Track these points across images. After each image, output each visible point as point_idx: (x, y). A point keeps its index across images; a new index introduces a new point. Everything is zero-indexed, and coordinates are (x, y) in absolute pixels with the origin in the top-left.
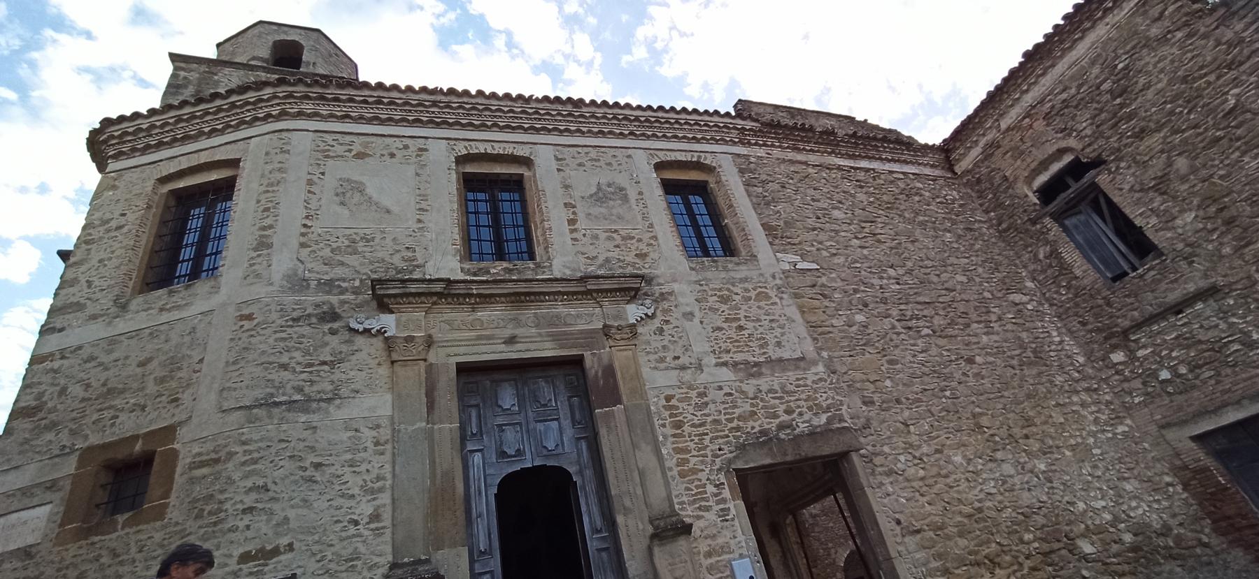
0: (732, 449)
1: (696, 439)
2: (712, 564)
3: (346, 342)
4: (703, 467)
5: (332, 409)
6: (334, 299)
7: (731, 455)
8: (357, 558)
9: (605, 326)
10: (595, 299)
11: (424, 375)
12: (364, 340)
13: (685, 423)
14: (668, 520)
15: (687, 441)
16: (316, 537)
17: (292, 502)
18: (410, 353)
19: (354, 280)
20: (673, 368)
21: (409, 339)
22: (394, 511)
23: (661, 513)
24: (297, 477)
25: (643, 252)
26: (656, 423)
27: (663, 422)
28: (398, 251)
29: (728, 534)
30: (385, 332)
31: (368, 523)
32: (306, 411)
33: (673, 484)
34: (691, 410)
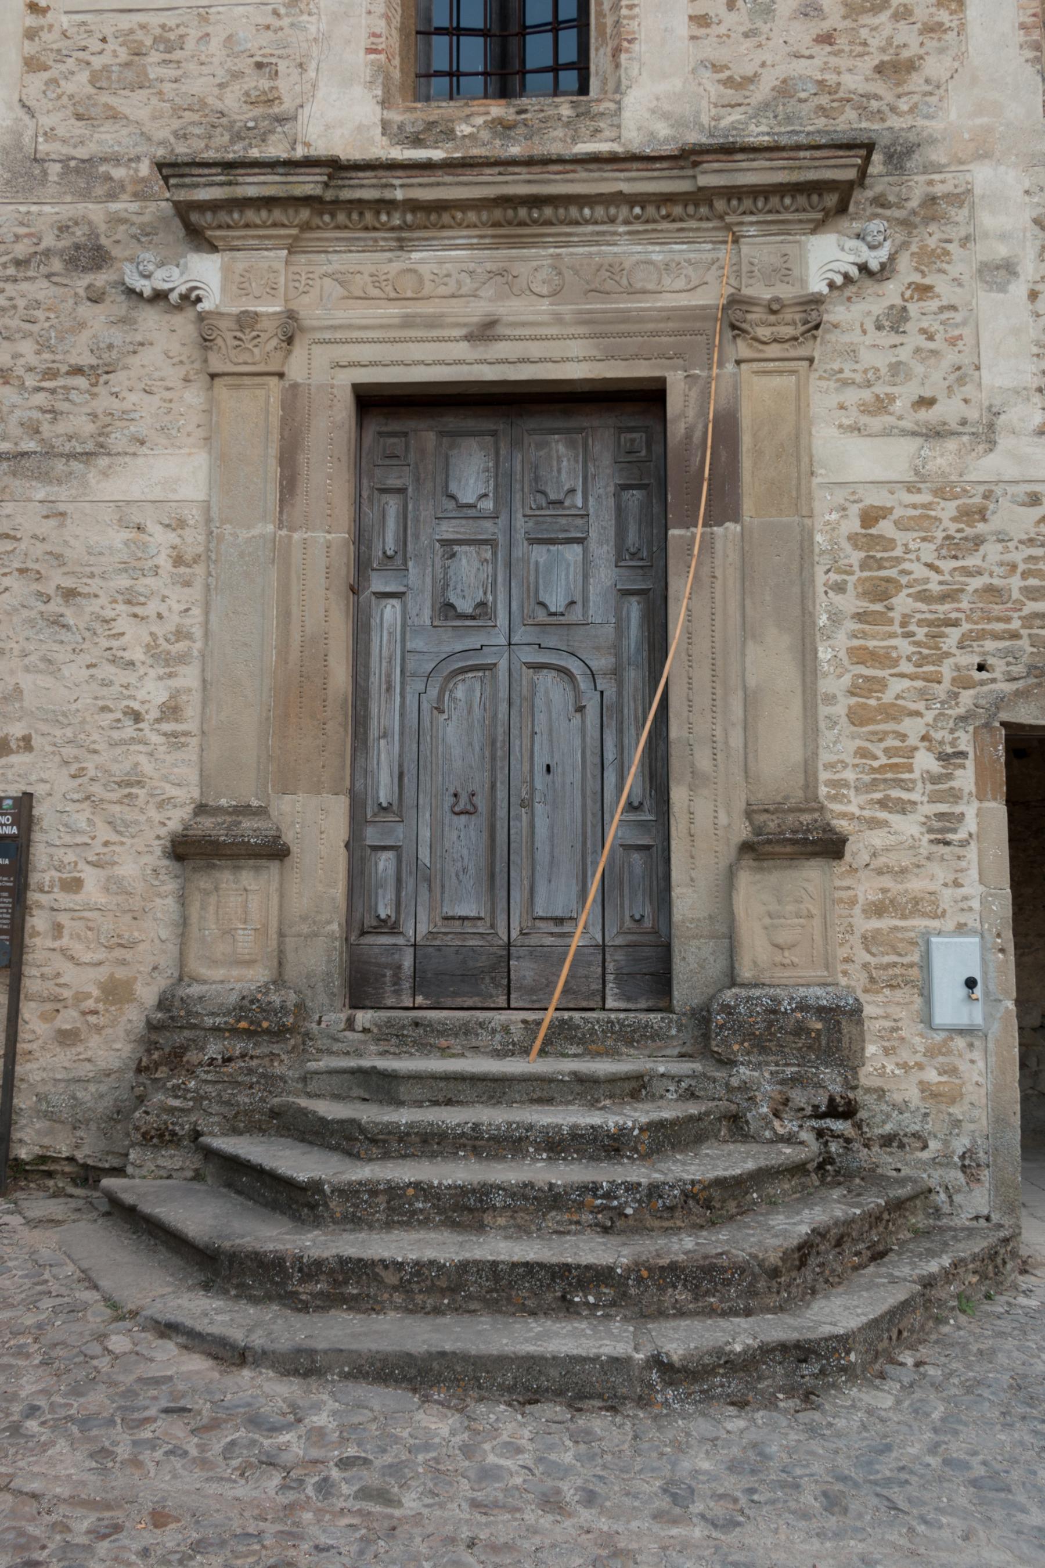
0: (1018, 670)
1: (921, 633)
2: (878, 931)
3: (123, 321)
4: (920, 706)
5: (92, 477)
6: (96, 212)
7: (1008, 687)
8: (139, 782)
9: (735, 302)
10: (721, 218)
11: (276, 412)
12: (157, 318)
13: (899, 587)
14: (790, 818)
15: (892, 635)
16: (69, 733)
17: (26, 661)
18: (246, 357)
19: (138, 159)
20: (905, 433)
21: (246, 321)
22: (204, 703)
23: (779, 799)
24: (33, 614)
25: (905, 54)
26: (820, 578)
27: (838, 578)
28: (237, 75)
29: (941, 873)
30: (199, 300)
31: (158, 721)
32: (45, 477)
33: (827, 737)
34: (928, 551)
